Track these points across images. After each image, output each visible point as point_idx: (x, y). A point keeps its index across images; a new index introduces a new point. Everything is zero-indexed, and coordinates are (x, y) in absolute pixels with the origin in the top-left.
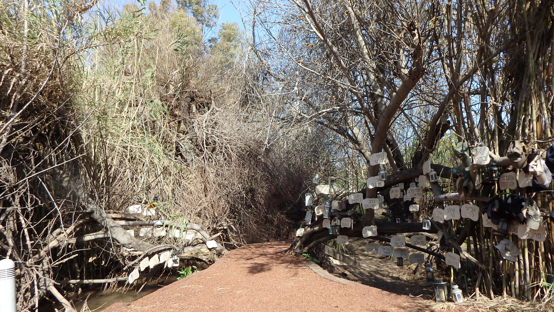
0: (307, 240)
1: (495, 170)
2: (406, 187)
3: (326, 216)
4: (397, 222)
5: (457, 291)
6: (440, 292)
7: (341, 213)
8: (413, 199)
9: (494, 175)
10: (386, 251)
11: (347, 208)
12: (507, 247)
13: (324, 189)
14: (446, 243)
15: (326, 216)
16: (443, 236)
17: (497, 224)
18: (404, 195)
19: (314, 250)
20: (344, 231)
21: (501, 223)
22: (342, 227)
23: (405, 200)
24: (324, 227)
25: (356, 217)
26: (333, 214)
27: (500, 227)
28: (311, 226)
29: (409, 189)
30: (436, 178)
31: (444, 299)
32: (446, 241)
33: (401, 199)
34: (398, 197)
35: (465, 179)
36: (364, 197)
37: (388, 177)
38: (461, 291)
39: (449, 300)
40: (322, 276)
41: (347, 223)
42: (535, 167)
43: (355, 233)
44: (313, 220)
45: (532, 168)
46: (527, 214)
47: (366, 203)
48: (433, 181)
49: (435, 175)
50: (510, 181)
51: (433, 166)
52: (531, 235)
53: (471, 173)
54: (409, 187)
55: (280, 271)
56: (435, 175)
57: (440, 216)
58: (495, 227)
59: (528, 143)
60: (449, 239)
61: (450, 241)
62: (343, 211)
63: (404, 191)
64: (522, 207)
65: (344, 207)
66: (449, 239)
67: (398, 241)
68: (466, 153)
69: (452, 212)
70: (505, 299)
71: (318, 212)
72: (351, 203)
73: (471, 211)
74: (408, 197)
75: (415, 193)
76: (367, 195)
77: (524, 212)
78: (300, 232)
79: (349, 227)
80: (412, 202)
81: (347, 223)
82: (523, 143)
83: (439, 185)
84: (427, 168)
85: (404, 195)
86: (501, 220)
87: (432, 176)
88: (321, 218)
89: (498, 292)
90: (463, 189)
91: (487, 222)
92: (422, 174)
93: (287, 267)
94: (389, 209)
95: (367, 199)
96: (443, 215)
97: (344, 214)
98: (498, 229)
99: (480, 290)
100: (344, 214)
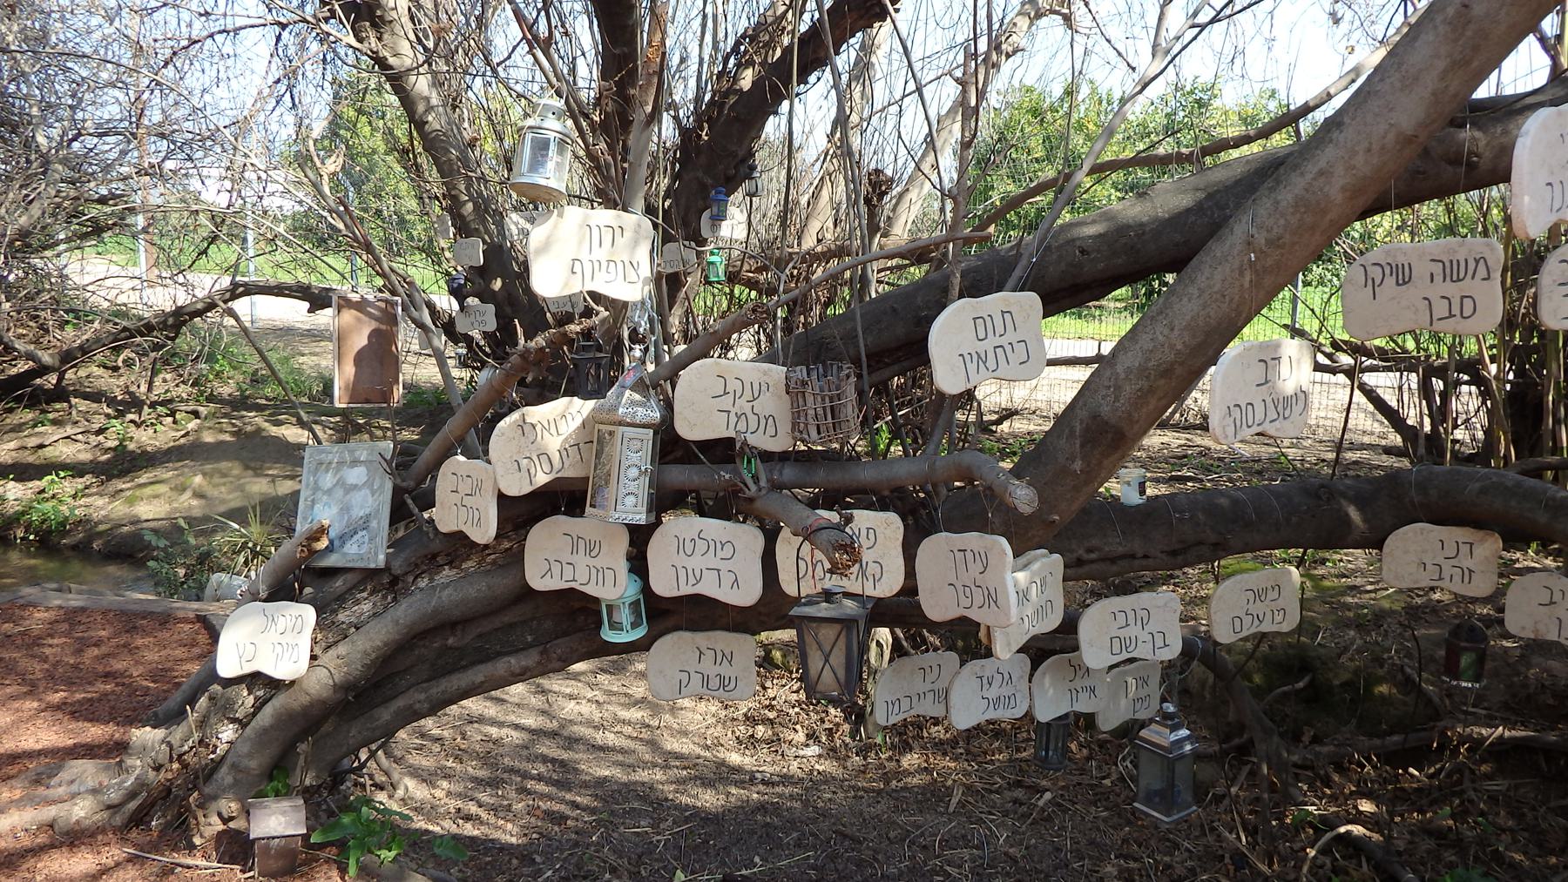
67: (1134, 631)
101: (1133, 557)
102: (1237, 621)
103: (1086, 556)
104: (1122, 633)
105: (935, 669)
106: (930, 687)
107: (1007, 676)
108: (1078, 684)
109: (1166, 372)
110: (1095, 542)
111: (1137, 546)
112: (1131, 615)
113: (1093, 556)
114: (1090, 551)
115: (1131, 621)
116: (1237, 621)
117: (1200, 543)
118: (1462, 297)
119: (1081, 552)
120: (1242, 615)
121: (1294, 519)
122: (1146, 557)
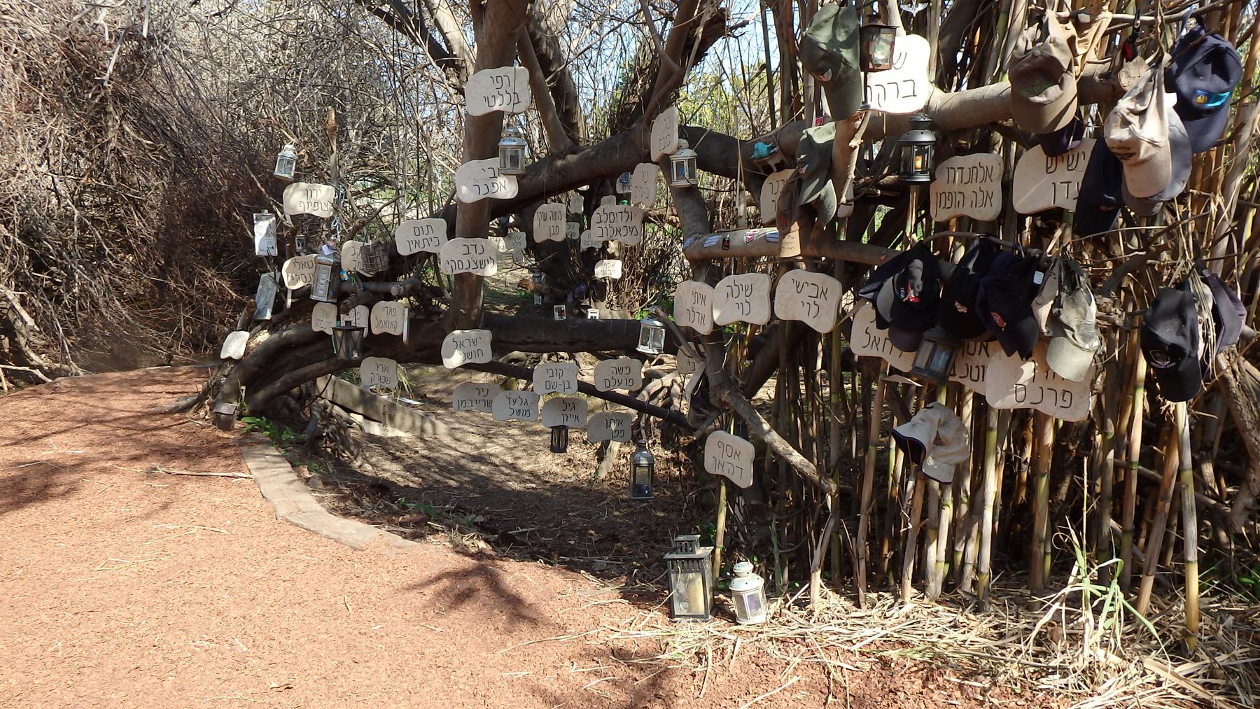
0: (258, 370)
1: (921, 145)
2: (592, 203)
3: (320, 294)
4: (557, 317)
5: (748, 580)
6: (689, 583)
7: (372, 286)
8: (606, 244)
9: (919, 164)
10: (517, 407)
11: (392, 269)
12: (942, 432)
13: (309, 200)
14: (712, 401)
15: (320, 294)
16: (704, 377)
17: (913, 347)
18: (581, 230)
19: (285, 407)
20: (380, 345)
21: (926, 348)
22: (376, 331)
23: (584, 247)
24: (316, 329)
25: (423, 297)
26: (345, 287)
27: (922, 363)
28: (272, 326)
29: (599, 210)
30: (692, 175)
31: (700, 607)
32: (711, 393)
33: (576, 243)
34: (559, 238)
35: (811, 177)
36: (451, 234)
37: (534, 168)
38: (761, 581)
39: (718, 609)
40: (282, 511)
41: (391, 319)
42: (1134, 120)
43: (421, 348)
44: (279, 305)
45: (1126, 123)
46: (1054, 319)
47: (454, 256)
48: (683, 183)
49: (690, 162)
50: (975, 186)
51: (684, 132)
52: (1034, 396)
53: (836, 151)
54: (597, 206)
55: (116, 492)
56: (690, 162)
57: (699, 307)
58: (900, 360)
59: (1088, 26)
60: (721, 386)
61: (725, 396)
62: (379, 277)
63: (580, 221)
64: (1036, 290)
65: (382, 263)
66: (721, 386)
67: (555, 379)
68: (847, 54)
69: (742, 298)
70: (908, 608)
71: (293, 276)
72: (403, 250)
73: (812, 301)
74: (591, 239)
75: (619, 223)
76: (458, 227)
77: (1044, 312)
78: (236, 345)
79: (397, 333)
80: (602, 253)
81: (392, 317)
82: (1070, 25)
83: (700, 200)
84: (664, 136)
85: (581, 230)
86: (926, 334)
87: (680, 165)
88: (304, 300)
89: (884, 579)
90: (797, 213)
91: (866, 340)
92: (647, 158)
93: (151, 474)
94: (541, 270)
95: (458, 241)
96: (714, 306)
97: (381, 287)
98: (915, 368)
99: (822, 576)
100: (381, 287)
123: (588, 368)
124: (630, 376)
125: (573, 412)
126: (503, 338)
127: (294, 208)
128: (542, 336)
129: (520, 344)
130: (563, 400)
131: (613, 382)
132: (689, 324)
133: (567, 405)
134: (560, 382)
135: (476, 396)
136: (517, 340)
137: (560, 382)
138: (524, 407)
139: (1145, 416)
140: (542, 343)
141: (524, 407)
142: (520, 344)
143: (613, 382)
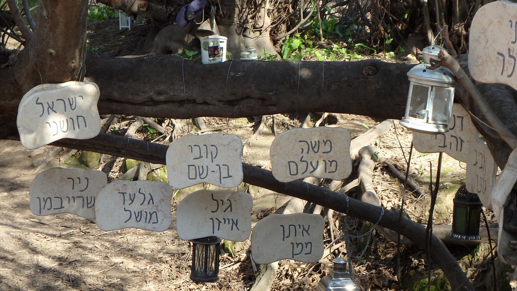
10: (136, 207)
67: (205, 162)
101: (194, 101)
102: (293, 166)
103: (156, 98)
104: (197, 163)
105: (84, 182)
106: (80, 194)
107: (148, 198)
108: (220, 215)
109: (13, 184)
110: (162, 87)
111: (195, 93)
112: (203, 149)
113: (162, 98)
114: (159, 93)
115: (204, 154)
116: (293, 166)
117: (248, 97)
118: (78, 117)
119: (151, 94)
120: (297, 161)
121: (333, 87)
122: (205, 103)
123: (258, 142)
124: (332, 156)
125: (228, 215)
126: (116, 95)
127: (193, 8)
128: (182, 92)
129: (143, 104)
130: (212, 194)
131: (302, 166)
132: (503, 80)
133: (216, 202)
134: (213, 167)
135: (68, 190)
136: (139, 99)
137: (213, 167)
138: (147, 208)
139: (435, 6)
140: (181, 102)
141: (147, 208)
142: (143, 104)
143: (302, 166)
